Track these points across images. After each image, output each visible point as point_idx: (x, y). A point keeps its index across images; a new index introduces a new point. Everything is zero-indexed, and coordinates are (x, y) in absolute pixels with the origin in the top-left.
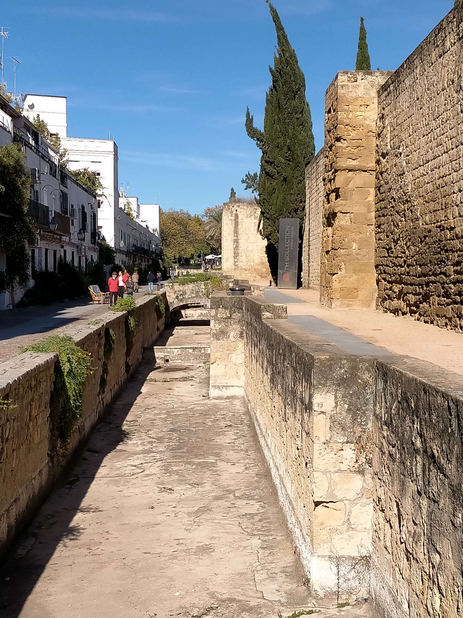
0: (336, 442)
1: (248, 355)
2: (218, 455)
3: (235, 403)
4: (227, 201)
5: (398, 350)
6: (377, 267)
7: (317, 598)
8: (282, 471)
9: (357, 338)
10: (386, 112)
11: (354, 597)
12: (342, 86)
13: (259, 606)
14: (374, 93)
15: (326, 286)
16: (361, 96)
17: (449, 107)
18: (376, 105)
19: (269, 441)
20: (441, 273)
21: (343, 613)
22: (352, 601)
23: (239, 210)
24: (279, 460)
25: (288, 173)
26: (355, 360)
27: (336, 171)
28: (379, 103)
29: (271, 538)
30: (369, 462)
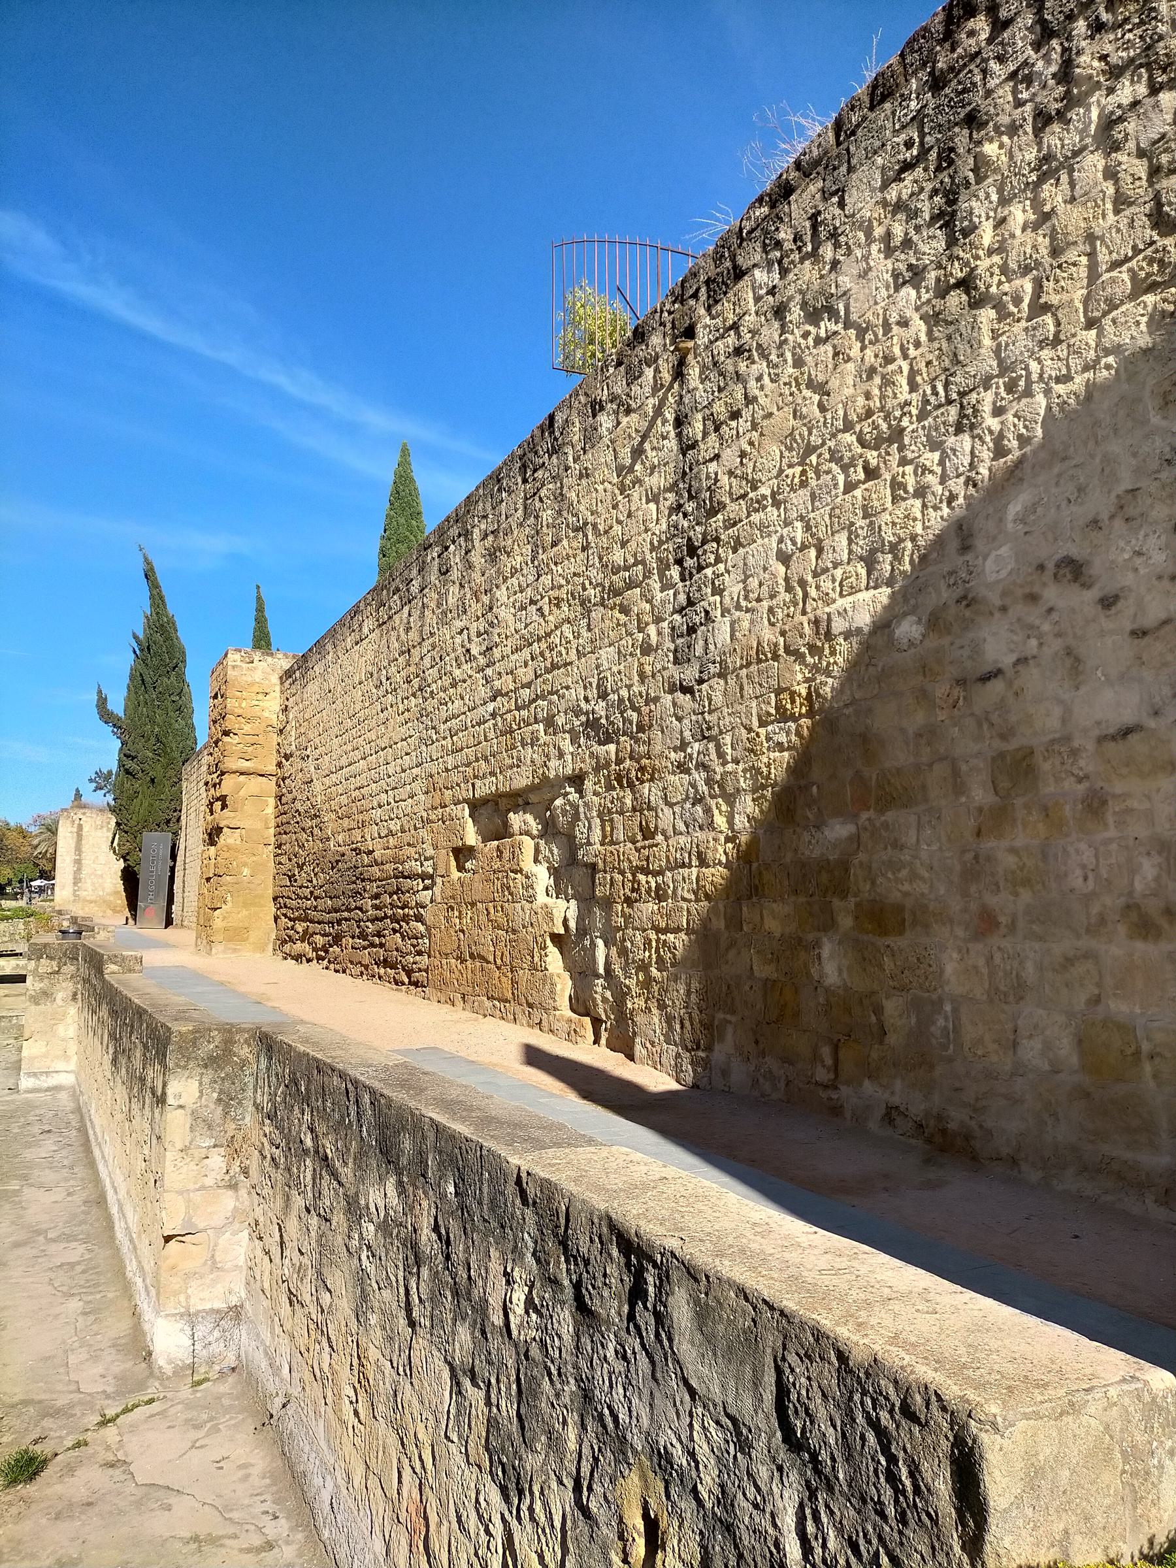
0: (200, 1147)
1: (82, 1025)
2: (25, 1178)
3: (59, 1096)
4: (68, 805)
5: (294, 1010)
6: (275, 899)
7: (162, 1378)
8: (122, 1193)
9: (243, 996)
10: (290, 704)
11: (217, 1368)
12: (233, 667)
13: (71, 1406)
14: (275, 679)
15: (205, 926)
16: (257, 681)
17: (367, 705)
18: (278, 694)
19: (106, 1151)
20: (356, 908)
21: (198, 1395)
22: (213, 1375)
23: (84, 818)
24: (119, 1179)
25: (157, 771)
26: (230, 1031)
27: (223, 774)
28: (282, 692)
29: (98, 1296)
30: (245, 1172)
